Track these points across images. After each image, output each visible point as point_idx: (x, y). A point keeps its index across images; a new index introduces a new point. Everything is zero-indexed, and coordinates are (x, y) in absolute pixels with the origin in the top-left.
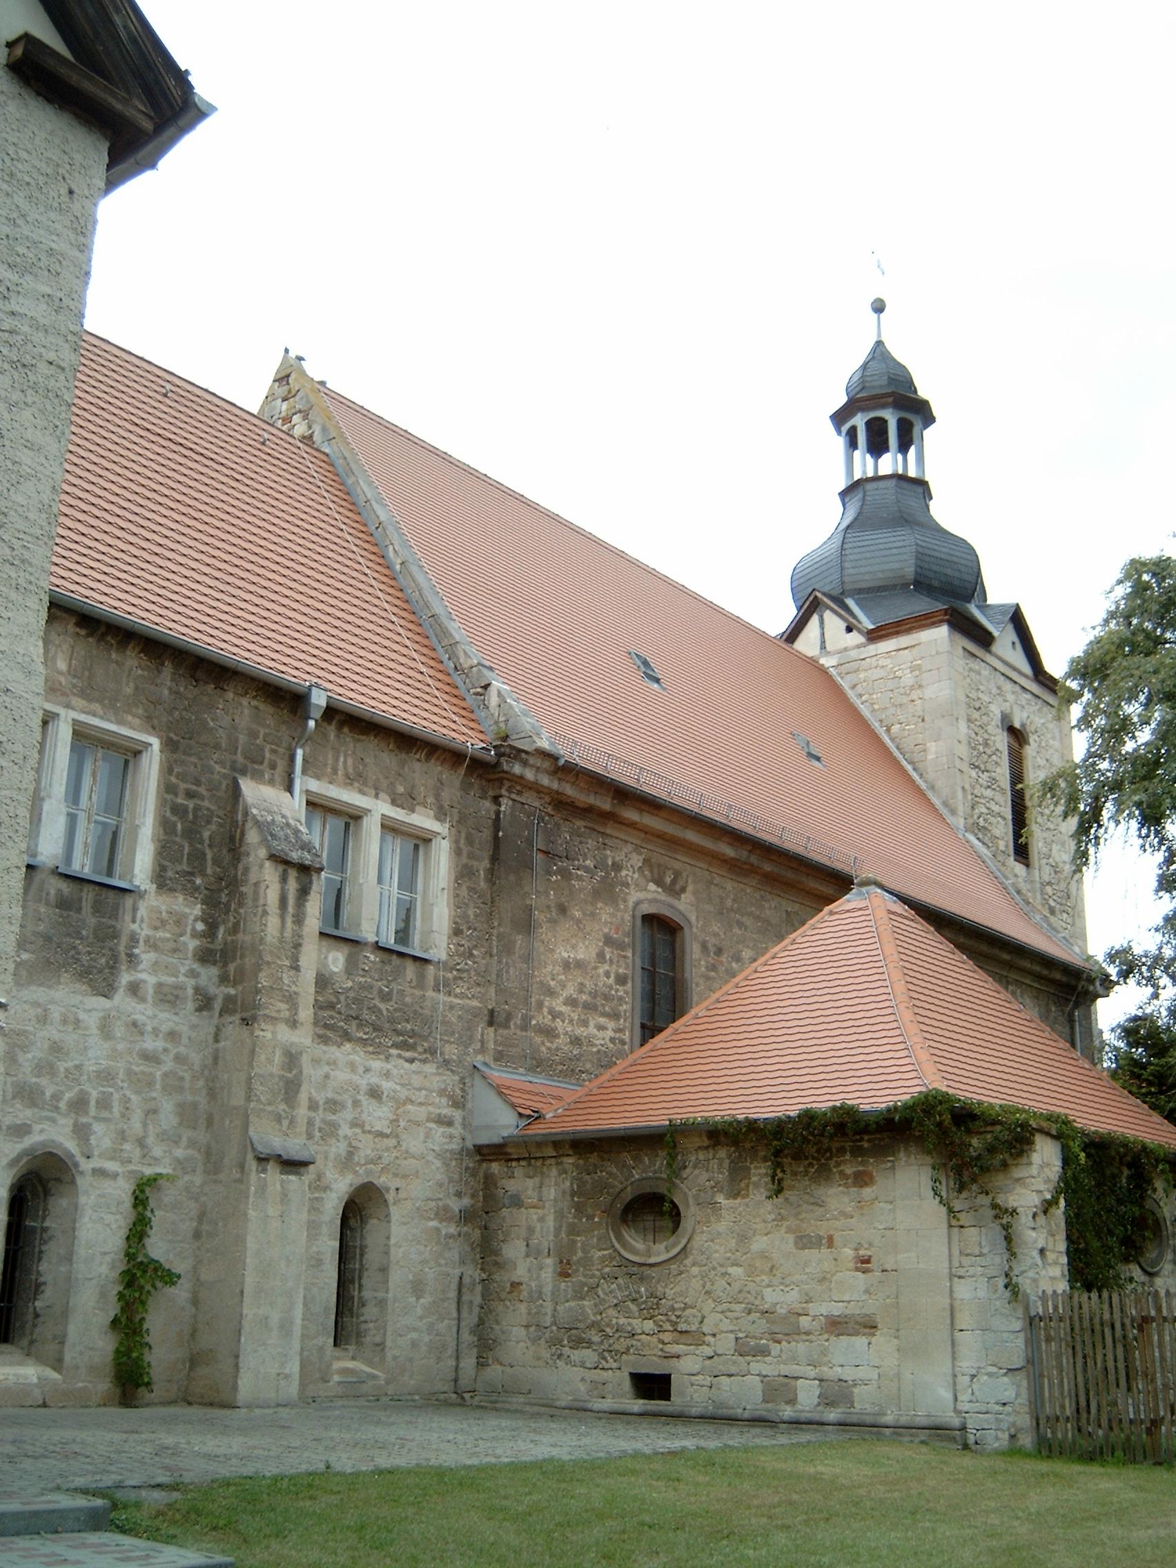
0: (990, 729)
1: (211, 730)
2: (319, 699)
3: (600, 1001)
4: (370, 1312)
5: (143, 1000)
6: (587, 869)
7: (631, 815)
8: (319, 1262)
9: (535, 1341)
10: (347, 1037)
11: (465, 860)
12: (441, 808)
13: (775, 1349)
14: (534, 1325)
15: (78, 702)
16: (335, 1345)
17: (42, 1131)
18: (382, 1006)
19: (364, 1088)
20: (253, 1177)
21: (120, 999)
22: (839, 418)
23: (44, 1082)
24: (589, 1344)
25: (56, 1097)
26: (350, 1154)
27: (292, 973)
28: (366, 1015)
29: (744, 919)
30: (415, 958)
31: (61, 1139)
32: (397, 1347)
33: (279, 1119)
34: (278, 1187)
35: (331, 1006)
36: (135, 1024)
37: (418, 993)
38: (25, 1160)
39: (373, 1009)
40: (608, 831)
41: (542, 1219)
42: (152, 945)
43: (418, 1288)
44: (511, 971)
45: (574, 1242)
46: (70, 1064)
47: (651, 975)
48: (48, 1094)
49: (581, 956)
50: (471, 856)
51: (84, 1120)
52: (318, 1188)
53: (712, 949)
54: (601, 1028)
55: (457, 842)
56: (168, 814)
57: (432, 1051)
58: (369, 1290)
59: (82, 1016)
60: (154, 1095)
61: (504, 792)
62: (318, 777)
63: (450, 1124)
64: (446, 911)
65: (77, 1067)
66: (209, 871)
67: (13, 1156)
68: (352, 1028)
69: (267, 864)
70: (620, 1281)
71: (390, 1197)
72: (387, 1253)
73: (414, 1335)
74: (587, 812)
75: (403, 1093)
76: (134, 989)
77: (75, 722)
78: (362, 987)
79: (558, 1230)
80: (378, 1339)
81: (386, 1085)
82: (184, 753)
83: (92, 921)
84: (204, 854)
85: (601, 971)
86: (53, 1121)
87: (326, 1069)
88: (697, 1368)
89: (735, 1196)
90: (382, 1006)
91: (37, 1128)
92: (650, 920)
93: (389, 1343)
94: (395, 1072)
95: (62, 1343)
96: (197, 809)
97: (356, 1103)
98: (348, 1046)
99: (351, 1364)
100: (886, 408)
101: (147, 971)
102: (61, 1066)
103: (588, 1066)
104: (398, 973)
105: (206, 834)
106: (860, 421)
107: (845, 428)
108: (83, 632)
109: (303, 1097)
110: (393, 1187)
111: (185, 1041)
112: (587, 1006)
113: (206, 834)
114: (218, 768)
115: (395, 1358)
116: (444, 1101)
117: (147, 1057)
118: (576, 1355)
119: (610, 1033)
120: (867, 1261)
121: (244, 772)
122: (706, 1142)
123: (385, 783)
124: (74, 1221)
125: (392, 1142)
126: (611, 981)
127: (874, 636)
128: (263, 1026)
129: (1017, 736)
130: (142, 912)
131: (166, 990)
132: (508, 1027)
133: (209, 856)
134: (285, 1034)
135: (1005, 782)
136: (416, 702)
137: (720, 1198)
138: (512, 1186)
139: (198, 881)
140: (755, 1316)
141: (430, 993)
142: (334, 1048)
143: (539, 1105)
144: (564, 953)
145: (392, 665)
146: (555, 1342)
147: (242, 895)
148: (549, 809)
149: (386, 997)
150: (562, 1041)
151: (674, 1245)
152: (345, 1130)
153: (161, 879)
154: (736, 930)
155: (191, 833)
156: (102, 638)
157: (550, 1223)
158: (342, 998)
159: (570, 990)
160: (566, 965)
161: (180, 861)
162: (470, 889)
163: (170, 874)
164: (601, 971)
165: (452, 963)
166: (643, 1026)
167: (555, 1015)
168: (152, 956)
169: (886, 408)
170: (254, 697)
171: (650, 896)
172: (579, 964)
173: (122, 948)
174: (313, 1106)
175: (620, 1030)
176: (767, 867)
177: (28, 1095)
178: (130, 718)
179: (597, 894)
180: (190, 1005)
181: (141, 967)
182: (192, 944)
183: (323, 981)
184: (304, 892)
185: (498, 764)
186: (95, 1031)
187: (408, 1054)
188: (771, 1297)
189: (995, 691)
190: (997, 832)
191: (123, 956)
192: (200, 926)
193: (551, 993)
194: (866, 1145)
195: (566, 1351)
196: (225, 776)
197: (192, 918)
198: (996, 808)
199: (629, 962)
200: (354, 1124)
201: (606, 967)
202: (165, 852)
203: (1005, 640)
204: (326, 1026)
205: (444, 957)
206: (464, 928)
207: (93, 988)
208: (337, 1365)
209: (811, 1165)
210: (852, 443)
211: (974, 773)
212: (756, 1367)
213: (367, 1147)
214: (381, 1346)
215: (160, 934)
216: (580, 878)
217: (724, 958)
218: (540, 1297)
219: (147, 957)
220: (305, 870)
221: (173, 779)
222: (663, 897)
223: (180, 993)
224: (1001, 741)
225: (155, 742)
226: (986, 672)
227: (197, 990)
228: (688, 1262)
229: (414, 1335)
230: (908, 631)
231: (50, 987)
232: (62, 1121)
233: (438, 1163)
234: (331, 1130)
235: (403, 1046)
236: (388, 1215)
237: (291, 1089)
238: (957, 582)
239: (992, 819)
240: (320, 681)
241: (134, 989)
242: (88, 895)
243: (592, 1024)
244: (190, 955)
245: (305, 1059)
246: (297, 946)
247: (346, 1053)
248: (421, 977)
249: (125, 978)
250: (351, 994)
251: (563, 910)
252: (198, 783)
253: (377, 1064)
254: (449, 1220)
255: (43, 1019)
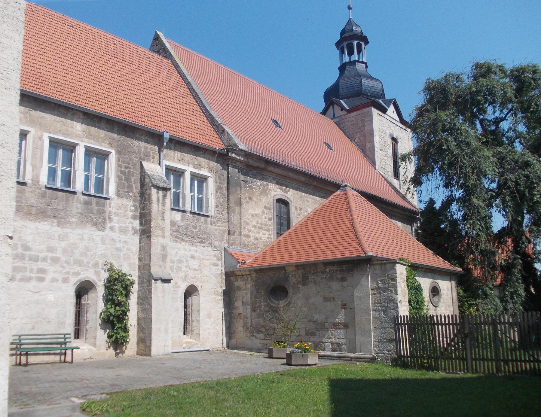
0: (386, 138)
1: (132, 147)
2: (167, 136)
3: (263, 226)
4: (195, 324)
5: (115, 232)
6: (258, 186)
7: (271, 168)
8: (178, 310)
9: (246, 331)
10: (183, 240)
11: (218, 184)
12: (210, 168)
13: (318, 333)
14: (245, 325)
15: (84, 139)
16: (184, 334)
17: (84, 274)
18: (194, 230)
19: (189, 256)
20: (153, 285)
21: (107, 231)
22: (338, 44)
23: (83, 258)
24: (262, 332)
25: (88, 263)
26: (186, 276)
27: (163, 221)
28: (189, 233)
29: (309, 199)
30: (204, 216)
31: (90, 276)
32: (203, 334)
33: (161, 266)
34: (161, 288)
35: (177, 231)
36: (113, 239)
37: (205, 226)
38: (79, 283)
39: (191, 231)
40: (264, 174)
41: (246, 294)
42: (117, 215)
43: (209, 316)
44: (235, 218)
45: (256, 301)
46: (92, 253)
47: (279, 217)
48: (85, 262)
49: (257, 212)
50: (220, 183)
51: (98, 270)
52: (176, 287)
53: (299, 209)
54: (264, 234)
55: (215, 179)
56: (119, 174)
57: (211, 244)
58: (194, 317)
59: (95, 237)
60: (121, 261)
61: (230, 163)
62: (169, 160)
63: (217, 265)
64: (213, 201)
65: (94, 253)
66: (134, 191)
67: (75, 282)
68: (184, 237)
69: (152, 188)
70: (270, 312)
71: (199, 289)
72: (199, 306)
73: (209, 330)
74: (257, 168)
75: (202, 257)
76: (112, 228)
77: (85, 146)
78: (187, 225)
79: (251, 298)
80: (198, 332)
81: (197, 255)
82: (123, 154)
83: (96, 208)
84: (132, 186)
85: (263, 217)
86: (87, 270)
87: (177, 250)
88: (294, 339)
89: (304, 286)
90: (194, 230)
91: (82, 273)
92: (279, 201)
93: (201, 333)
94: (199, 250)
95: (95, 339)
96: (129, 172)
97: (187, 260)
98: (183, 243)
99: (189, 340)
100: (351, 40)
101: (116, 223)
102: (89, 253)
103: (260, 246)
104: (198, 220)
105: (133, 180)
106: (345, 44)
107: (340, 47)
108: (85, 118)
109: (168, 259)
110: (200, 286)
111: (130, 244)
112: (259, 228)
113: (133, 180)
114: (135, 159)
115: (203, 338)
116: (215, 258)
117: (117, 249)
118: (258, 336)
119: (267, 236)
120: (345, 305)
121: (144, 160)
122: (295, 269)
123: (191, 161)
124: (97, 301)
125: (199, 272)
126: (267, 219)
127: (349, 111)
128: (154, 238)
129: (395, 140)
130: (113, 205)
131: (122, 228)
132: (234, 235)
133: (134, 186)
134: (161, 240)
135: (391, 154)
136: (201, 136)
137: (300, 286)
138: (236, 284)
139: (131, 194)
140: (311, 323)
141: (209, 226)
142: (179, 244)
143: (244, 259)
144: (251, 212)
145: (193, 125)
146: (251, 332)
147: (145, 198)
148: (245, 168)
149: (195, 228)
150: (252, 239)
151: (286, 301)
152: (184, 269)
153: (118, 195)
154: (306, 203)
155: (128, 179)
156: (92, 119)
157: (249, 295)
158: (181, 228)
159: (254, 223)
160: (252, 215)
161: (124, 188)
162: (221, 193)
163: (121, 192)
164: (263, 217)
165: (216, 216)
166: (277, 233)
167: (249, 231)
168: (117, 218)
169: (351, 40)
170: (146, 136)
171: (278, 193)
172: (256, 215)
173: (107, 216)
174: (172, 262)
175: (270, 235)
176: (315, 184)
177: (79, 263)
178: (104, 144)
179: (261, 193)
180: (131, 233)
181: (113, 222)
182: (130, 214)
183: (173, 223)
184: (165, 196)
185: (228, 154)
186: (100, 242)
187: (203, 245)
188: (316, 317)
189: (387, 126)
190: (388, 170)
191: (107, 219)
192: (133, 208)
193: (248, 224)
194: (344, 268)
195: (255, 334)
196: (138, 161)
197: (129, 206)
198: (388, 163)
199: (272, 214)
200: (186, 267)
201: (265, 215)
202: (119, 185)
203: (391, 110)
204: (176, 237)
205: (213, 214)
206: (219, 205)
207: (98, 229)
208: (184, 340)
209: (327, 275)
210: (342, 52)
211: (381, 152)
212: (312, 339)
213: (191, 274)
214: (199, 334)
215: (119, 211)
216: (256, 189)
217: (302, 211)
218: (247, 318)
219: (115, 219)
220: (165, 189)
221: (120, 163)
222: (282, 193)
223: (127, 229)
224: (390, 142)
225: (113, 152)
226: (385, 120)
227: (133, 228)
228: (291, 306)
229: (209, 330)
230: (360, 109)
231: (83, 229)
232: (90, 270)
233: (214, 278)
234: (179, 269)
235: (202, 242)
236: (199, 294)
237: (164, 257)
238: (375, 93)
239: (387, 166)
240: (167, 130)
241: (112, 228)
242: (94, 200)
243: (261, 233)
244: (130, 217)
245: (168, 248)
246: (163, 213)
247: (183, 245)
248: (206, 221)
249: (108, 225)
250: (184, 227)
251: (250, 198)
252: (129, 164)
253: (193, 248)
254: (218, 295)
255: (82, 239)
